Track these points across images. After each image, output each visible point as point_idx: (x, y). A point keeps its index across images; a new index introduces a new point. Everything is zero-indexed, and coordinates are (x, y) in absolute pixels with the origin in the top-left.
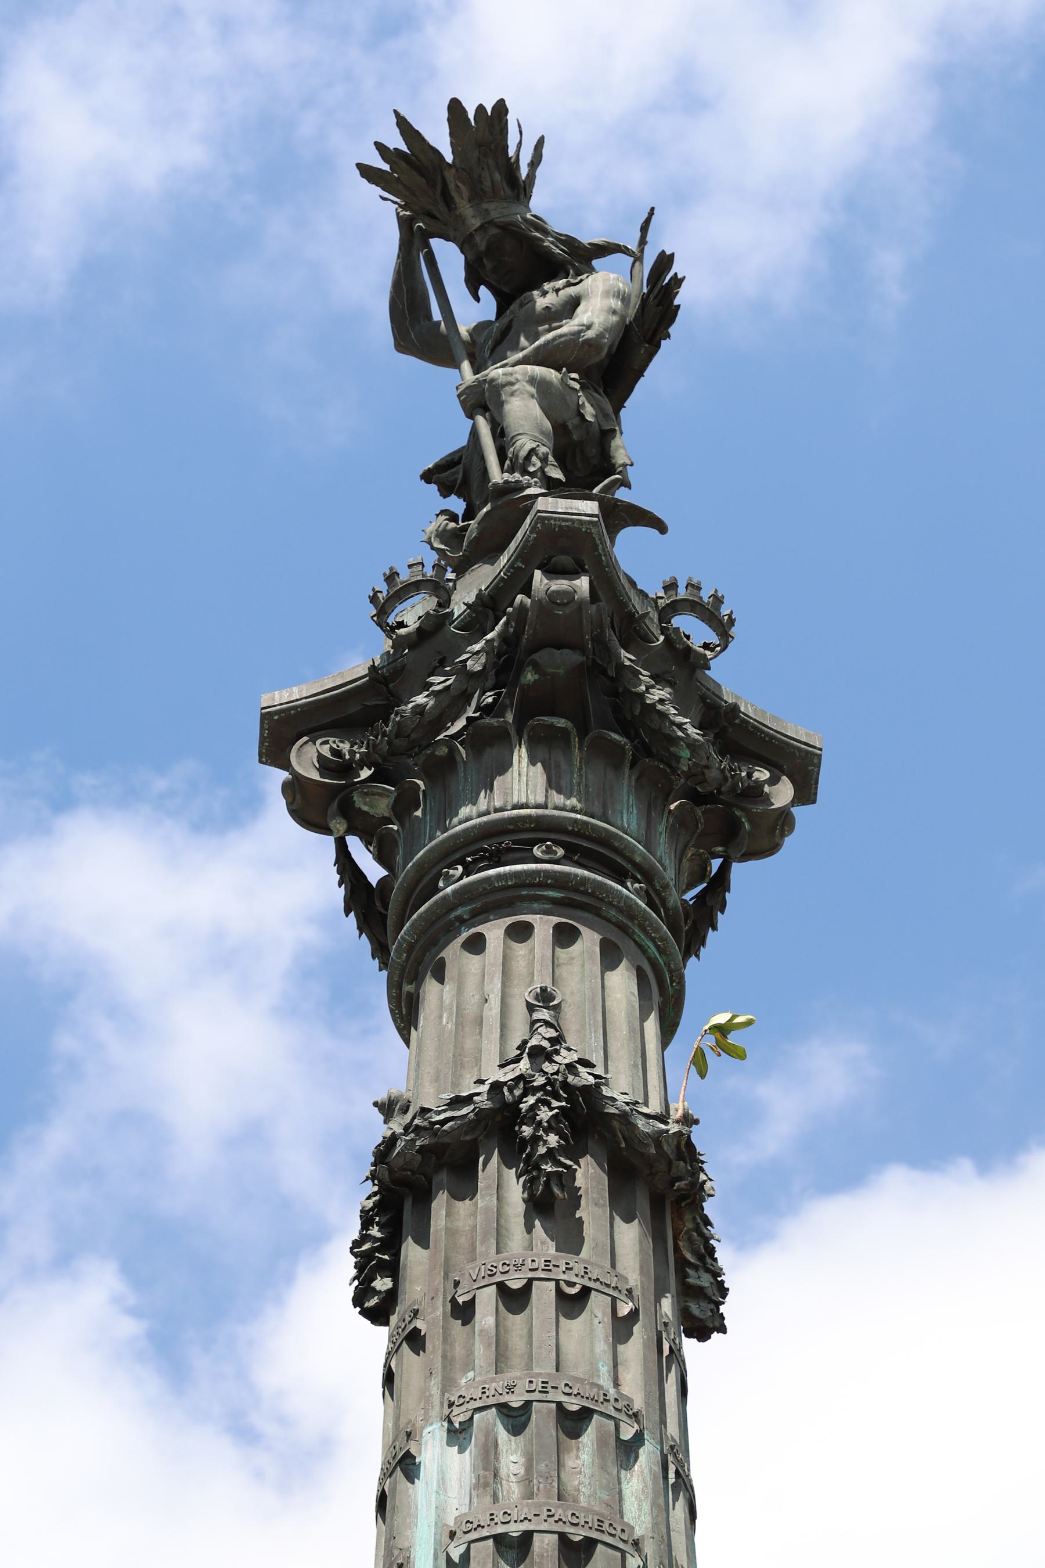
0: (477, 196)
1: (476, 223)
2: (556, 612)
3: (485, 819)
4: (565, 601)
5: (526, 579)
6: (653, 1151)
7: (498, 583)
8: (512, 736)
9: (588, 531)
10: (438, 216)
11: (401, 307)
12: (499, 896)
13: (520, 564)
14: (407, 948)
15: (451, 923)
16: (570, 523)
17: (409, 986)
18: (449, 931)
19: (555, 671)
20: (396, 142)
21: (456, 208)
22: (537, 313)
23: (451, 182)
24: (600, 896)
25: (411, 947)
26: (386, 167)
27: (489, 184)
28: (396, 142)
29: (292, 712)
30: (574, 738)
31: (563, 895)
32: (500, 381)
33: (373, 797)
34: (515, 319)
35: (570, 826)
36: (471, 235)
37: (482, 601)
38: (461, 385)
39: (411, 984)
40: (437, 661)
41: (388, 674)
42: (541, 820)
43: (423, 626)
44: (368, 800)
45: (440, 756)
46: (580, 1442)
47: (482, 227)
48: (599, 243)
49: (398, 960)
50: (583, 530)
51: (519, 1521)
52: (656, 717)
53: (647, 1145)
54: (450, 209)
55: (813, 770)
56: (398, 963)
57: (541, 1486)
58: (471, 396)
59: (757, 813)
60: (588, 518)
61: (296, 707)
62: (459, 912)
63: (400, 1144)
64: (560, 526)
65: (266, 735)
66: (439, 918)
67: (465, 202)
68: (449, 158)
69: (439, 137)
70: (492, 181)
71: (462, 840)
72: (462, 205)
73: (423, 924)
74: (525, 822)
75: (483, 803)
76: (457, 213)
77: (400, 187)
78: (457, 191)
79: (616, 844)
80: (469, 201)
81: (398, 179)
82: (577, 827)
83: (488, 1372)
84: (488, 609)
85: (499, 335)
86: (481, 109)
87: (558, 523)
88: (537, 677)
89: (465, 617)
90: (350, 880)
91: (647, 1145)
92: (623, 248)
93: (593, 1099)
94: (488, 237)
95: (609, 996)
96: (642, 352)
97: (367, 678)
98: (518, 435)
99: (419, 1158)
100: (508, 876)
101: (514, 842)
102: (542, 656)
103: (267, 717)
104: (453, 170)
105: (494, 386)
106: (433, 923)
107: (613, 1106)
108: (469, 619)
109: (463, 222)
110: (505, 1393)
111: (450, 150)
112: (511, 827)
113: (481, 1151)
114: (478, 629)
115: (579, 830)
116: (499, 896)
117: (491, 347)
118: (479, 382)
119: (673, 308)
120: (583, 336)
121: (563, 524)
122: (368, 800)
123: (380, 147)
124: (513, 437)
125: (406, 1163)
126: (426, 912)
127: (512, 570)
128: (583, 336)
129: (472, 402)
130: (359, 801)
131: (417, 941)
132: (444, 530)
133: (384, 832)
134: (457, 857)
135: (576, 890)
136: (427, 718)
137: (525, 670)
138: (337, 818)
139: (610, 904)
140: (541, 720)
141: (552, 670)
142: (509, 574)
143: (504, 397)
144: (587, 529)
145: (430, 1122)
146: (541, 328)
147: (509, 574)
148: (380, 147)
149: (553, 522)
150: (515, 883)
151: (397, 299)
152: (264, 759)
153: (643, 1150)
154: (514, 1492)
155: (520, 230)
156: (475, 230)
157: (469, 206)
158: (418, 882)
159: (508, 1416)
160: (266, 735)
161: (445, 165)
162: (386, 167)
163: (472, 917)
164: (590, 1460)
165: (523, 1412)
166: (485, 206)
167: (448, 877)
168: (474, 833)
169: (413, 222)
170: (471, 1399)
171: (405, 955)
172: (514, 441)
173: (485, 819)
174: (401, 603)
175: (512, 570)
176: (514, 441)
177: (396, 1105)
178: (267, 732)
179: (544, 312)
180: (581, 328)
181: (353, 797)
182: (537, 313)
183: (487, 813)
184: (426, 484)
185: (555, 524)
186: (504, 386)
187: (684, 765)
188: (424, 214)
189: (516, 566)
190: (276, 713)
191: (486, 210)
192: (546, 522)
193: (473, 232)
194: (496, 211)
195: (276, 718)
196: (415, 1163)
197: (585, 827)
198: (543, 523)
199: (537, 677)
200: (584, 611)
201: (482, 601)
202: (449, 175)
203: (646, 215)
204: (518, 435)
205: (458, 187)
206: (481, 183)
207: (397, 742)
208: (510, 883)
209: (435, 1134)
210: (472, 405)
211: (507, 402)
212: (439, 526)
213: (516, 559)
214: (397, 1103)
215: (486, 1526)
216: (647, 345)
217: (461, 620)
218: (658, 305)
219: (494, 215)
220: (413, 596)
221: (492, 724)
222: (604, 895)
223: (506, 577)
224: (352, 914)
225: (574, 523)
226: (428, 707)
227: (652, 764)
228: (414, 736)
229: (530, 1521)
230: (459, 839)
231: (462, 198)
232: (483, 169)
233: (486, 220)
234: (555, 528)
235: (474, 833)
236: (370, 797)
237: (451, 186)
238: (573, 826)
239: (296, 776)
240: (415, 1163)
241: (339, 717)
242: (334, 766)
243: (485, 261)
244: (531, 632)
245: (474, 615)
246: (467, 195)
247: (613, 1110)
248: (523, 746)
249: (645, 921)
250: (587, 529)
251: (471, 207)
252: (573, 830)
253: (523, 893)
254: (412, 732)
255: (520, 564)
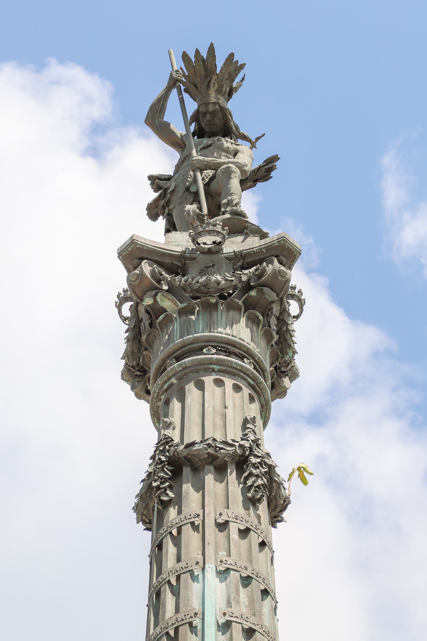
0: (219, 91)
1: (214, 100)
2: (279, 277)
3: (228, 336)
4: (284, 276)
5: (262, 257)
6: (282, 502)
7: (251, 251)
8: (242, 311)
9: (296, 255)
10: (199, 88)
11: (157, 108)
12: (233, 370)
13: (264, 250)
14: (184, 367)
15: (209, 369)
16: (292, 248)
17: (175, 380)
18: (206, 371)
19: (268, 298)
20: (204, 54)
21: (209, 90)
22: (224, 147)
23: (213, 80)
24: (263, 391)
25: (186, 368)
26: (193, 60)
27: (225, 90)
28: (204, 54)
29: (145, 248)
30: (261, 326)
31: (253, 383)
32: (233, 169)
33: (165, 298)
34: (214, 144)
35: (257, 358)
36: (209, 103)
37: (241, 254)
38: (196, 157)
39: (176, 380)
40: (212, 264)
41: (187, 257)
42: (249, 350)
43: (212, 248)
44: (162, 298)
45: (211, 302)
46: (263, 603)
47: (214, 103)
48: (246, 135)
49: (177, 369)
50: (295, 253)
51: (252, 623)
52: (289, 335)
53: (281, 499)
54: (207, 89)
55: (292, 380)
56: (176, 370)
57: (258, 613)
58: (199, 163)
59: (281, 386)
60: (299, 250)
61: (148, 247)
62: (215, 366)
63: (196, 447)
64: (288, 247)
65: (129, 249)
66: (204, 364)
67: (214, 90)
68: (218, 72)
69: (220, 63)
70: (226, 89)
71: (218, 339)
72: (212, 91)
73: (197, 362)
74: (244, 347)
75: (228, 330)
76: (208, 92)
77: (193, 70)
78: (213, 85)
79: (266, 374)
80: (215, 91)
81: (194, 66)
82: (259, 360)
83: (236, 557)
84: (241, 258)
85: (206, 146)
86: (237, 62)
87: (289, 245)
88: (255, 295)
89: (230, 255)
90: (135, 321)
91: (281, 499)
92: (252, 142)
93: (271, 471)
94: (215, 108)
95: (201, 417)
96: (249, 184)
97: (180, 253)
98: (235, 193)
99: (206, 456)
100: (239, 365)
101: (239, 353)
102: (266, 290)
103: (135, 244)
104: (217, 77)
105: (230, 170)
106: (201, 364)
107: (278, 478)
108: (231, 257)
109: (209, 97)
110: (244, 569)
111: (220, 69)
112: (238, 346)
113: (228, 467)
114: (233, 263)
115: (259, 362)
116: (233, 370)
117: (201, 148)
118: (204, 160)
119: (270, 176)
120: (244, 168)
121: (290, 247)
122: (162, 298)
123: (197, 51)
124: (232, 193)
125: (198, 455)
126: (201, 359)
127: (260, 250)
128: (244, 168)
129: (198, 166)
130: (159, 296)
131: (190, 367)
132: (195, 211)
133: (169, 314)
134: (213, 344)
135: (257, 384)
136: (220, 287)
137: (254, 290)
138: (151, 298)
139: (264, 396)
140: (256, 312)
141: (268, 297)
142: (258, 251)
143: (232, 176)
144: (296, 254)
145: (215, 445)
146: (223, 153)
147: (258, 251)
148: (197, 51)
149: (287, 244)
150: (240, 369)
151: (157, 105)
152: (121, 257)
153: (279, 500)
154: (243, 610)
155: (226, 113)
156: (212, 103)
157: (214, 92)
158: (191, 344)
159: (242, 579)
160: (129, 249)
161: (215, 73)
162: (193, 60)
163: (218, 371)
164: (268, 612)
165: (246, 580)
166: (219, 96)
167: (209, 350)
168: (224, 340)
169: (177, 82)
170: (231, 564)
171: (181, 369)
172: (232, 195)
173: (228, 336)
174: (210, 235)
175: (260, 250)
176: (232, 195)
177: (172, 425)
178: (130, 249)
179: (226, 148)
180: (245, 164)
181: (158, 294)
182: (224, 147)
183: (229, 335)
184: (148, 179)
185: (287, 245)
186: (234, 172)
187: (287, 358)
188: (192, 84)
189: (262, 250)
190: (139, 244)
191: (219, 98)
192: (285, 242)
193: (210, 103)
194: (222, 101)
195: (138, 246)
196: (202, 457)
197: (261, 362)
198: (284, 242)
199: (255, 295)
200: (287, 283)
201: (241, 254)
202: (214, 77)
203: (261, 135)
204: (235, 193)
205: (215, 84)
206: (222, 87)
207: (203, 288)
208: (238, 368)
209: (216, 451)
210: (197, 167)
211: (233, 179)
212: (194, 208)
213: (264, 248)
214: (173, 424)
215: (239, 618)
216: (252, 183)
217: (228, 255)
218: (265, 172)
219: (221, 102)
220: (215, 236)
221: (239, 303)
222: (264, 392)
223: (256, 251)
224: (127, 334)
225: (293, 249)
226: (221, 283)
227: (276, 350)
228: (211, 290)
229: (255, 625)
230: (218, 339)
231: (214, 88)
232: (225, 83)
233: (217, 102)
234: (286, 246)
235: (224, 340)
236: (164, 297)
237: (212, 82)
238: (258, 359)
239: (142, 274)
240: (202, 457)
241: (160, 260)
242: (157, 278)
243: (208, 115)
244: (266, 279)
245: (234, 257)
246: (216, 88)
247: (277, 480)
248: (244, 317)
249: (269, 409)
250: (296, 254)
251: (215, 93)
252: (257, 360)
253: (241, 374)
254: (211, 288)
255: (264, 250)
